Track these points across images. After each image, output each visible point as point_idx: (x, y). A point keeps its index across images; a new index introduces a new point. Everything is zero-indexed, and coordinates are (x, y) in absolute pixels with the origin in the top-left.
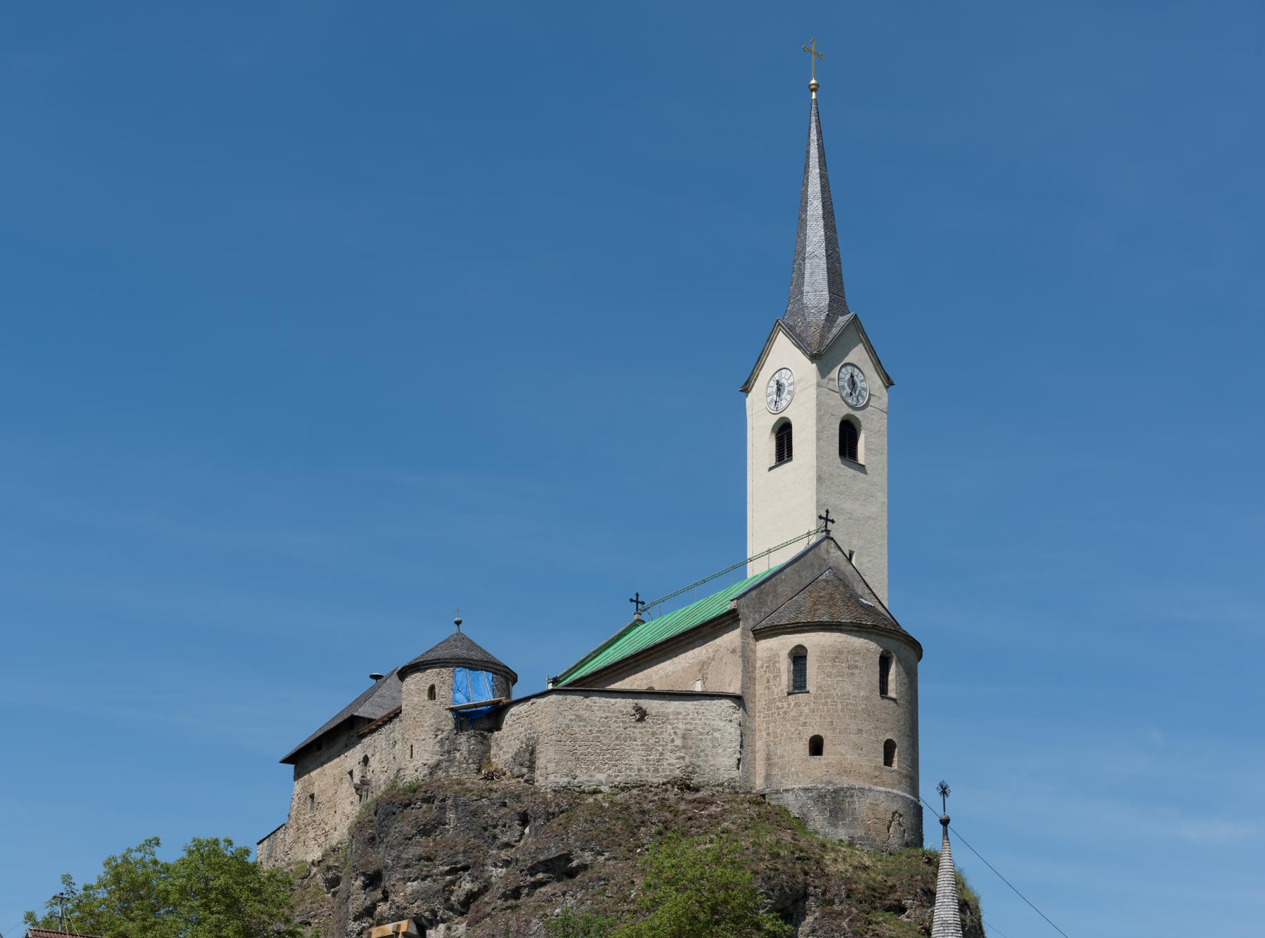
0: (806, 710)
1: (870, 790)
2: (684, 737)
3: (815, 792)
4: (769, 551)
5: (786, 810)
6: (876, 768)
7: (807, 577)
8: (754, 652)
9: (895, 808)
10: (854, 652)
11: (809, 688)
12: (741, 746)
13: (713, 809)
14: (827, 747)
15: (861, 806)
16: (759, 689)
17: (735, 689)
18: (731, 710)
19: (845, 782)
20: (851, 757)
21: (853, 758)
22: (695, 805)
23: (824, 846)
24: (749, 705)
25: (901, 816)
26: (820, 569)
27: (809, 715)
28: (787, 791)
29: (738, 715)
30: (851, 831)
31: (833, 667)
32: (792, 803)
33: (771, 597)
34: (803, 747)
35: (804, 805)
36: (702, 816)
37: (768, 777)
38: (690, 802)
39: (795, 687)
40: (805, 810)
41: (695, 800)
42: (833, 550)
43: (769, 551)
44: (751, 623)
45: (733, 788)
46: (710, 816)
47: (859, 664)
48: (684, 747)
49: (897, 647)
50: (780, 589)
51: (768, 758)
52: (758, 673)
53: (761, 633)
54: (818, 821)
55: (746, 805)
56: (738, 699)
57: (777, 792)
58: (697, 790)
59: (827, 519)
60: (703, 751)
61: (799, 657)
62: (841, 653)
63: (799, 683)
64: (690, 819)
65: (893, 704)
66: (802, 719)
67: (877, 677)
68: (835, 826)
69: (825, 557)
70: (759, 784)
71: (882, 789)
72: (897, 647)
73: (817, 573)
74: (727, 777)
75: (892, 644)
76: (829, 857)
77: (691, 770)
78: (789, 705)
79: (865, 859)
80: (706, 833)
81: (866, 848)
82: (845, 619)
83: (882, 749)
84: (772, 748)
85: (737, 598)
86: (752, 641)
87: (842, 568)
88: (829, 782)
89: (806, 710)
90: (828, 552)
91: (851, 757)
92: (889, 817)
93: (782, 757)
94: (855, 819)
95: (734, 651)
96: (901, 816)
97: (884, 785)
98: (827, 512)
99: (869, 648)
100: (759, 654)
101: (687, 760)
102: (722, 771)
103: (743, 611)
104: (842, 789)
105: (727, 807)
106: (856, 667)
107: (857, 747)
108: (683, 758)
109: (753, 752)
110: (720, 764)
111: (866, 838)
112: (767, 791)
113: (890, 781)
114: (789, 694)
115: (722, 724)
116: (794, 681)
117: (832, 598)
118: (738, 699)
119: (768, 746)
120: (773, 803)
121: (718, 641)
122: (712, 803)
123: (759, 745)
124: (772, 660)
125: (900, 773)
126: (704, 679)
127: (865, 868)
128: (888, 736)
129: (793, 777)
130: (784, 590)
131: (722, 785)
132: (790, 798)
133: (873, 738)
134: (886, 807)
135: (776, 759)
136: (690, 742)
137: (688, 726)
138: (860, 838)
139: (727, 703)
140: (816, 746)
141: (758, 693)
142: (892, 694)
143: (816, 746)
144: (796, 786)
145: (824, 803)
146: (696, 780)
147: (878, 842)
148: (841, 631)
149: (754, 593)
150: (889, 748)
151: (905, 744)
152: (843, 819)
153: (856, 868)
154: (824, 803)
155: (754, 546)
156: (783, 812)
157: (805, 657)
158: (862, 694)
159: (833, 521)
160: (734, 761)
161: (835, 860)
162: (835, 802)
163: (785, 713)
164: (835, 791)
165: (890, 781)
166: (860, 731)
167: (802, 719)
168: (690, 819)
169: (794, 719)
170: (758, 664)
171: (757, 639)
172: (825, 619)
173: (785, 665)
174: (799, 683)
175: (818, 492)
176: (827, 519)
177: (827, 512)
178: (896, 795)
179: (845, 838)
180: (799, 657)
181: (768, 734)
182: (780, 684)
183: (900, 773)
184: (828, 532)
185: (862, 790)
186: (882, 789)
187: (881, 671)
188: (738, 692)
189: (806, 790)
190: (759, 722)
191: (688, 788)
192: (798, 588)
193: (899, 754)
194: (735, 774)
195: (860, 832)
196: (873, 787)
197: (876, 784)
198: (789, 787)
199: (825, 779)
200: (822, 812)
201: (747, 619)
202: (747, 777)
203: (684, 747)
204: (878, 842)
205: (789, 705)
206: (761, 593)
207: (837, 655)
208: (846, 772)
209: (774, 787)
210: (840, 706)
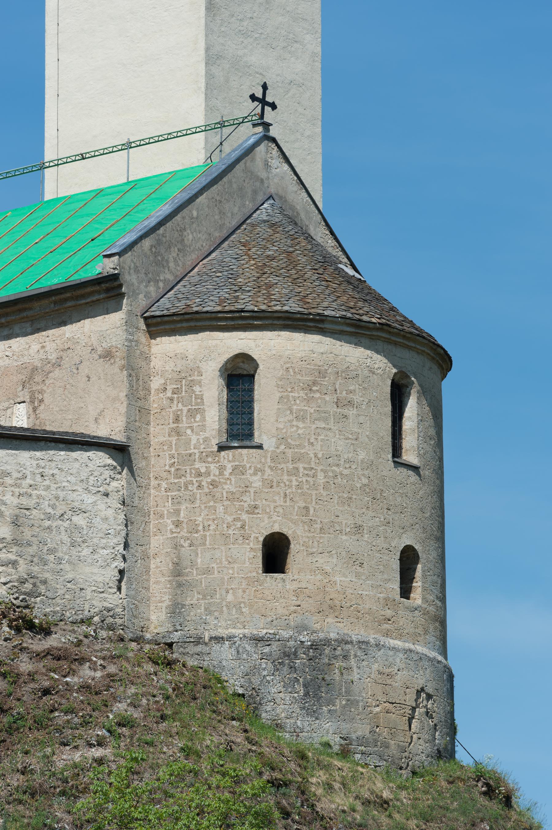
0: (256, 482)
1: (378, 645)
2: (16, 523)
3: (275, 646)
4: (129, 146)
5: (219, 681)
6: (388, 602)
7: (234, 212)
8: (147, 359)
9: (420, 682)
10: (347, 374)
11: (257, 438)
12: (126, 546)
13: (86, 673)
14: (296, 557)
15: (362, 676)
16: (158, 433)
17: (111, 428)
18: (107, 473)
19: (332, 628)
20: (343, 579)
21: (341, 581)
22: (48, 662)
23: (303, 757)
24: (139, 463)
25: (429, 697)
26: (253, 200)
27: (260, 492)
28: (219, 639)
29: (120, 483)
30: (345, 727)
31: (309, 400)
32: (231, 667)
33: (174, 252)
34: (252, 556)
35: (255, 670)
36: (69, 687)
37: (176, 610)
38: (39, 656)
39: (232, 435)
40: (256, 681)
41: (48, 653)
42: (276, 162)
43: (129, 146)
44: (142, 302)
45: (111, 628)
46: (85, 688)
47: (357, 398)
48: (16, 542)
49: (418, 360)
50: (189, 237)
51: (177, 571)
52: (155, 402)
53: (159, 325)
54: (281, 703)
55: (150, 668)
56: (120, 451)
57: (198, 641)
58: (45, 631)
59: (263, 102)
60: (51, 551)
61: (239, 376)
62: (322, 374)
63: (240, 427)
64: (46, 692)
65: (412, 477)
66: (248, 500)
67: (388, 422)
68: (314, 714)
69: (263, 175)
70: (157, 621)
71: (398, 643)
72: (418, 360)
73: (250, 206)
74: (99, 605)
75: (413, 361)
76: (318, 778)
77: (30, 587)
78: (222, 469)
79: (380, 785)
80: (85, 724)
81: (373, 760)
82: (331, 309)
83: (396, 565)
84: (186, 550)
85: (120, 254)
86: (143, 337)
87: (291, 197)
88: (301, 628)
89: (256, 482)
90: (267, 165)
91: (343, 579)
92: (410, 700)
93: (208, 571)
94: (352, 703)
95: (108, 355)
96: (429, 697)
97: (400, 637)
98: (265, 87)
99: (372, 365)
100: (156, 363)
101: (23, 567)
102: (88, 593)
103: (130, 280)
104: (327, 642)
105: (112, 669)
106: (350, 403)
107: (355, 561)
108: (14, 564)
109: (146, 557)
110: (84, 581)
111: (372, 741)
112: (176, 637)
113: (410, 629)
114: (221, 448)
115: (89, 499)
116: (230, 423)
117: (292, 263)
118: (120, 451)
119: (177, 547)
120: (191, 662)
121: (69, 330)
122: (81, 660)
123: (157, 543)
124: (185, 380)
125: (426, 613)
126: (35, 403)
127: (384, 804)
128: (407, 540)
129: (235, 615)
130: (197, 235)
131: (86, 621)
132: (224, 654)
133: (381, 542)
134: (410, 679)
135: (194, 575)
136: (28, 534)
137: (25, 501)
138: (362, 741)
139: (101, 458)
140: (275, 554)
141: (154, 441)
142: (410, 456)
143: (275, 554)
144: (238, 632)
145: (293, 668)
146: (40, 612)
147: (393, 750)
148: (322, 332)
149: (147, 243)
150: (408, 559)
151: (434, 554)
152: (331, 702)
153: (367, 803)
154: (293, 668)
155: (65, 125)
156: (212, 682)
157: (251, 377)
158: (362, 455)
159: (273, 106)
160: (112, 574)
161: (329, 787)
162: (314, 666)
163: (213, 484)
164: (314, 646)
165: (410, 629)
166: (358, 528)
167: (248, 500)
168: (46, 692)
169: (232, 497)
170: (156, 383)
171: (153, 335)
172: (293, 306)
173: (213, 393)
174: (240, 427)
175: (209, 31)
176: (263, 102)
177: (265, 87)
178: (422, 657)
179: (336, 741)
180: (239, 376)
181: (178, 524)
182: (203, 428)
183: (426, 613)
184: (267, 126)
185: (363, 644)
186: (398, 643)
187: (394, 412)
188: (119, 437)
189: (257, 640)
190: (157, 497)
191: (30, 626)
192: (218, 235)
193: (424, 576)
194: (113, 599)
195: (361, 729)
196: (383, 640)
197: (387, 634)
198: (222, 632)
199: (294, 620)
200: (289, 685)
201: (135, 294)
202: (135, 607)
203: (16, 542)
204: (393, 750)
205: (222, 469)
206: (159, 242)
207: (315, 379)
208: (334, 609)
209: (191, 629)
210: (321, 476)
